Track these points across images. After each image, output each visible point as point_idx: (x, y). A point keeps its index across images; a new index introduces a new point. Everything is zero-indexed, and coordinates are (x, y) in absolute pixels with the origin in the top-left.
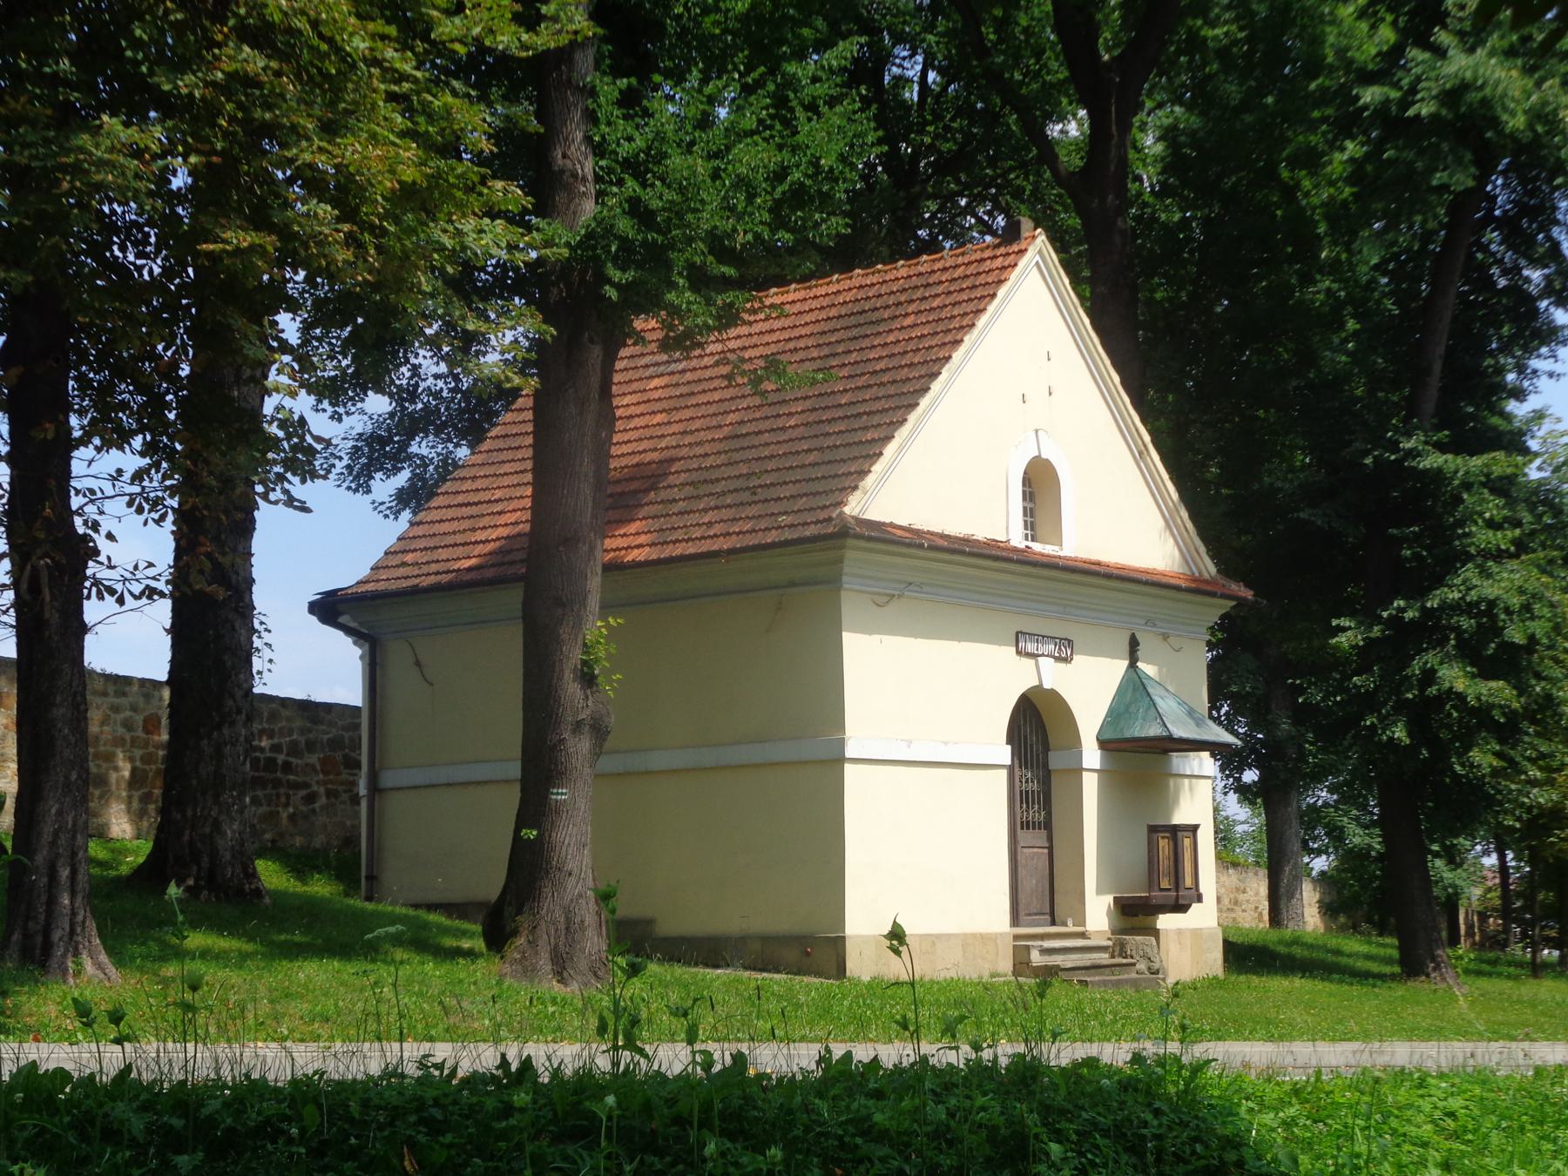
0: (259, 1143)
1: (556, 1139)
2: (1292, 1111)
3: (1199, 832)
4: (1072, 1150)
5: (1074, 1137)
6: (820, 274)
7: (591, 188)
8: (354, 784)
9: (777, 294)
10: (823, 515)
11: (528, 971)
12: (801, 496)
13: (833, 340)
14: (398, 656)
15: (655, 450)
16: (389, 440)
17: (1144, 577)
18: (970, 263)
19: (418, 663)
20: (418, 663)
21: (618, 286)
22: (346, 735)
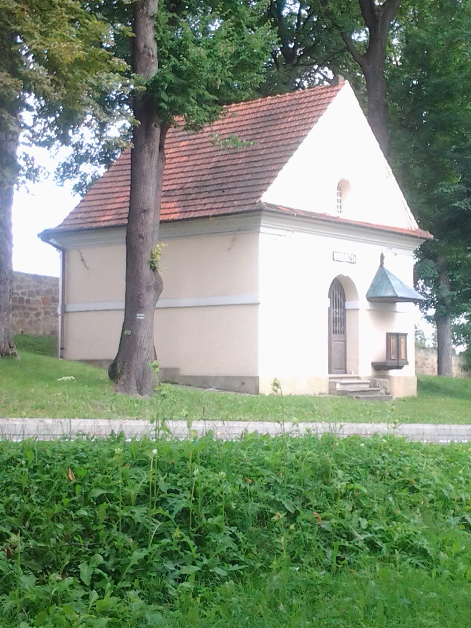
0: (9, 467)
1: (133, 466)
2: (441, 458)
3: (408, 336)
4: (348, 473)
5: (349, 468)
6: (252, 98)
7: (155, 60)
8: (56, 309)
9: (235, 106)
10: (252, 201)
11: (126, 389)
12: (243, 193)
13: (258, 127)
14: (74, 256)
15: (183, 172)
16: (72, 166)
17: (387, 229)
18: (317, 95)
19: (83, 260)
20: (83, 260)
21: (168, 104)
22: (53, 289)
